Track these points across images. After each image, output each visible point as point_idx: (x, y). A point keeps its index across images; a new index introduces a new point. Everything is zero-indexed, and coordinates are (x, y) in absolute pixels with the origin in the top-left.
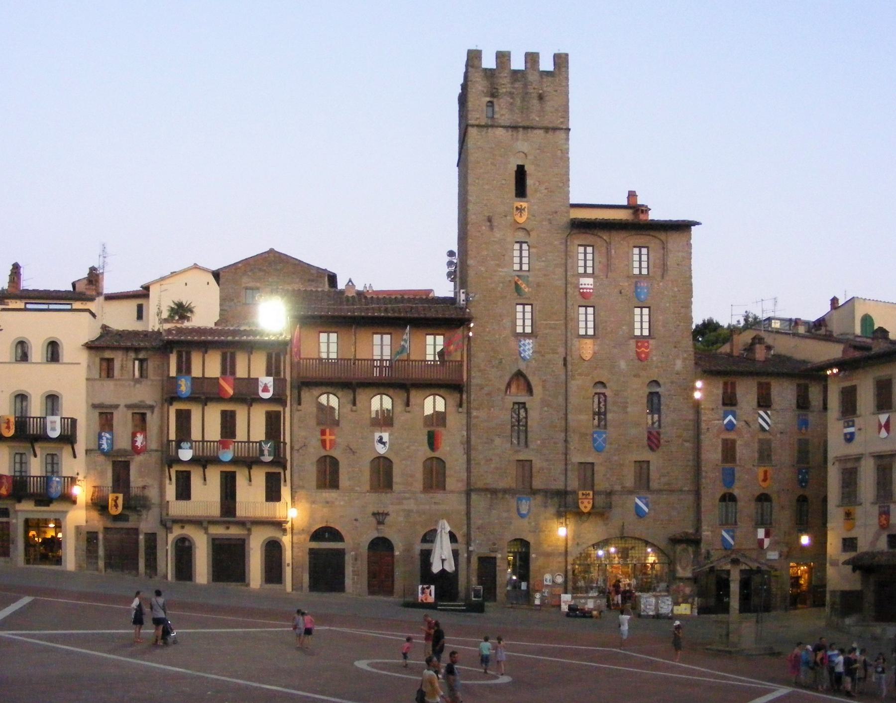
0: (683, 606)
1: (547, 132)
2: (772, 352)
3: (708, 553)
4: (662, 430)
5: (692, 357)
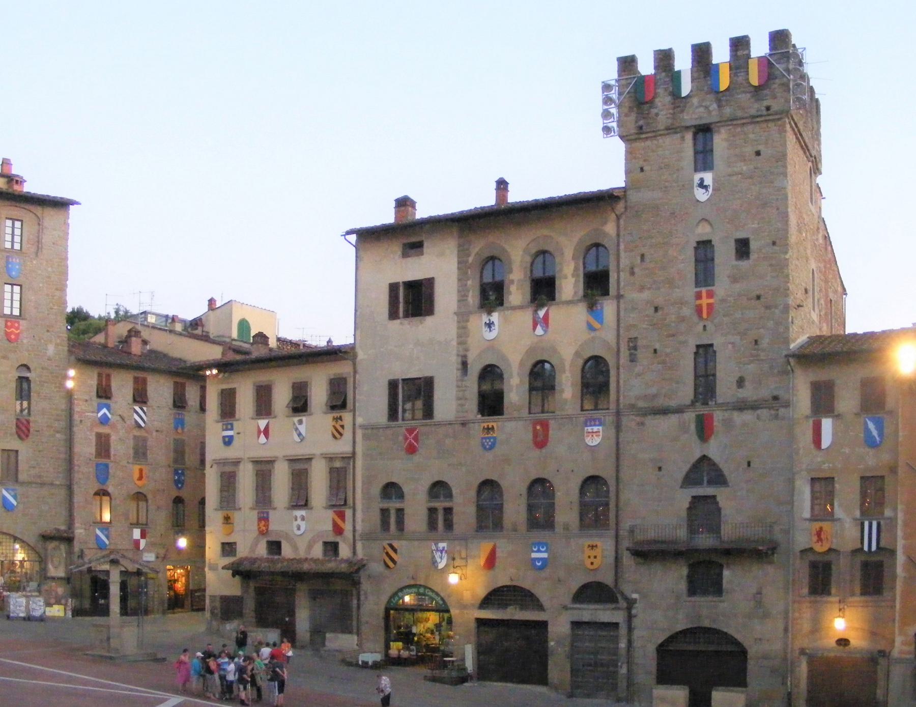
0: (56, 607)
2: (148, 347)
3: (82, 551)
4: (32, 419)
5: (66, 343)
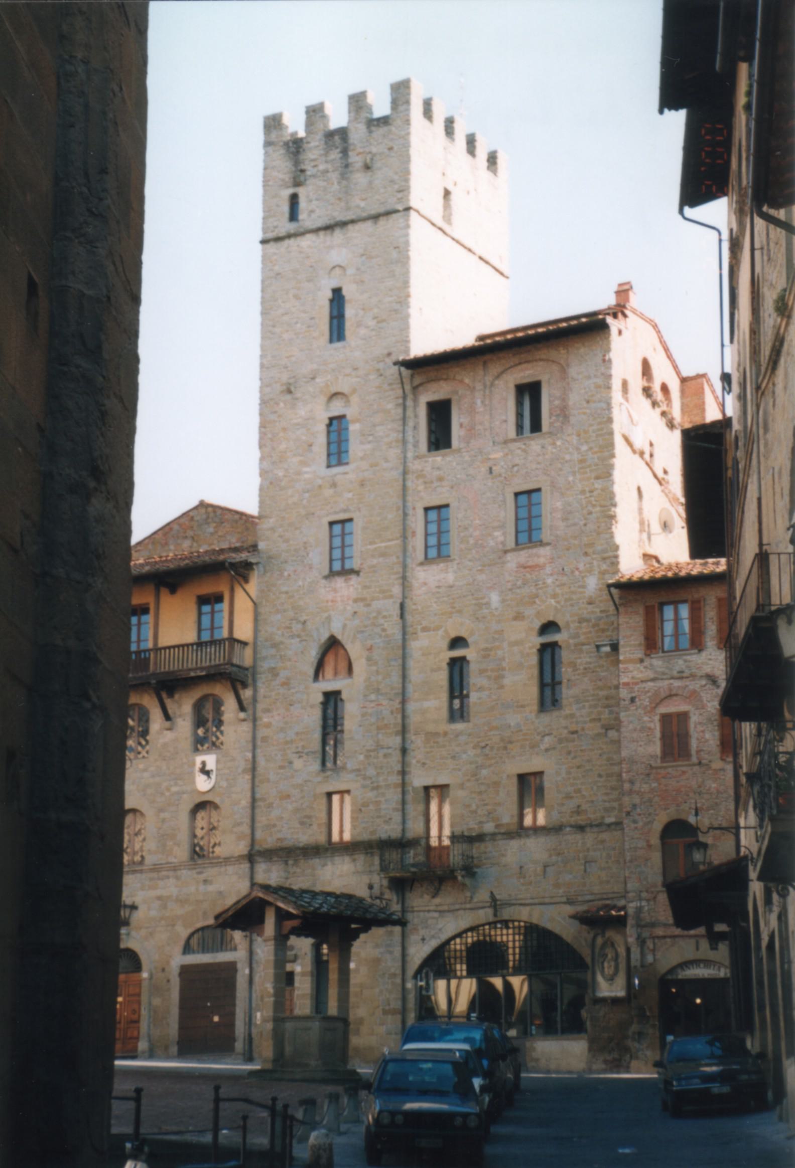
1: (376, 223)
